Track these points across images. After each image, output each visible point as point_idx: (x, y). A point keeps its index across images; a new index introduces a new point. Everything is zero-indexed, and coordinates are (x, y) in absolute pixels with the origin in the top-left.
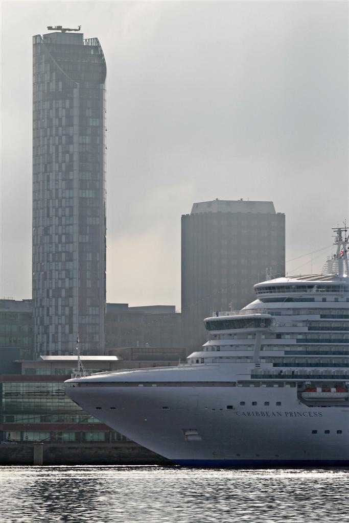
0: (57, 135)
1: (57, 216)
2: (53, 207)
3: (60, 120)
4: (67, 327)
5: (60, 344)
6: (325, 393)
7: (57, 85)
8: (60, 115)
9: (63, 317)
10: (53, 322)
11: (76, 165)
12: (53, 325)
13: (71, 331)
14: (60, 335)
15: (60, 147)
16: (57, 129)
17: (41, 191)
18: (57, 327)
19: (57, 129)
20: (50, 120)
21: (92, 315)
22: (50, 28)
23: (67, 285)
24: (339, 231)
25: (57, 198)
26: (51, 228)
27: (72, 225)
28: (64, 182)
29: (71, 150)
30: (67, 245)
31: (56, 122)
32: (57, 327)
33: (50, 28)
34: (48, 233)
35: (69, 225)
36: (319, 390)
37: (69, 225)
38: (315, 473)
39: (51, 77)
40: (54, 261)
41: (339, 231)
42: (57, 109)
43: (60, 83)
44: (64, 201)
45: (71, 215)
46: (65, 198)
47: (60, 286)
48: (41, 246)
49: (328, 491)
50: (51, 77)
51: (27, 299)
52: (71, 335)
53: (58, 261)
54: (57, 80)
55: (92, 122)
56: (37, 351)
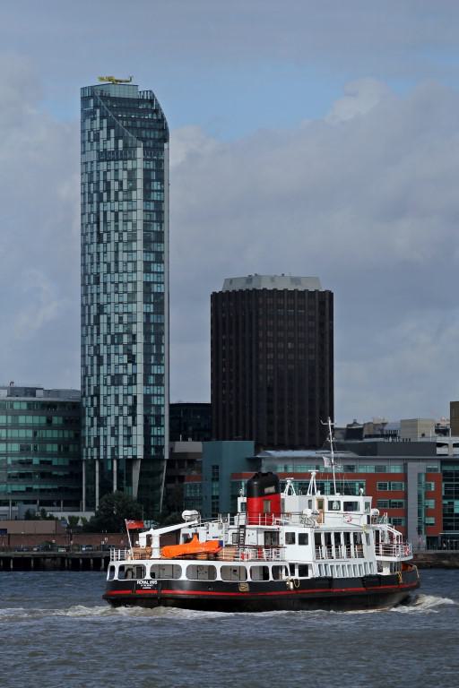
1: (116, 231)
3: (121, 184)
4: (130, 418)
7: (116, 143)
9: (125, 295)
10: (112, 239)
11: (140, 235)
12: (113, 243)
13: (134, 424)
16: (116, 193)
17: (95, 264)
19: (116, 193)
20: (108, 184)
21: (157, 273)
22: (102, 79)
23: (130, 371)
24: (355, 423)
26: (109, 418)
27: (136, 210)
29: (134, 218)
30: (130, 305)
31: (115, 186)
32: (117, 418)
33: (102, 79)
34: (105, 311)
38: (332, 421)
39: (109, 133)
40: (113, 384)
41: (355, 423)
42: (116, 171)
44: (121, 285)
45: (135, 271)
46: (122, 211)
47: (121, 372)
48: (95, 327)
50: (109, 133)
51: (80, 277)
52: (134, 428)
53: (118, 385)
55: (155, 370)
56: (89, 447)
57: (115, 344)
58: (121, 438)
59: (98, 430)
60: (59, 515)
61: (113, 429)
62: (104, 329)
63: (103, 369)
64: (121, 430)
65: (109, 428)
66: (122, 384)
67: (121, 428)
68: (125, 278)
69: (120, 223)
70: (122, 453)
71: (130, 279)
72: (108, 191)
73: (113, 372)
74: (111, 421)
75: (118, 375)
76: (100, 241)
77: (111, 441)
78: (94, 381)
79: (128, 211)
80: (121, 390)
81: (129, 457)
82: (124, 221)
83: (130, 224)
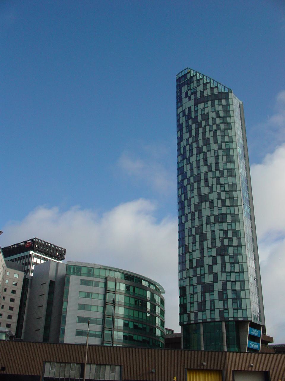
18: (224, 284)
46: (230, 281)
52: (243, 293)
57: (219, 223)
58: (230, 302)
59: (204, 296)
60: (165, 332)
61: (211, 268)
62: (206, 212)
63: (208, 244)
64: (230, 294)
65: (206, 267)
66: (226, 221)
67: (229, 292)
68: (233, 277)
69: (228, 266)
70: (230, 315)
71: (237, 278)
72: (207, 120)
73: (216, 212)
75: (222, 214)
76: (200, 150)
77: (219, 305)
78: (196, 255)
79: (235, 254)
80: (225, 226)
81: (240, 319)
82: (234, 309)
83: (236, 266)
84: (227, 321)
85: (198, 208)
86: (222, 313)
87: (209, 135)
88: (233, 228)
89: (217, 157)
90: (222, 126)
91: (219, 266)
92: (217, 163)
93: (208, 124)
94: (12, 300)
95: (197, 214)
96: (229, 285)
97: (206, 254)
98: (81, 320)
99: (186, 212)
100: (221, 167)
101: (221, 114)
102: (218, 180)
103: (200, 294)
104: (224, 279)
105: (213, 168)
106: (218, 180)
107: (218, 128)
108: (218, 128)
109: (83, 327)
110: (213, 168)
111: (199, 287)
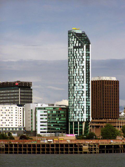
0: (70, 84)
2: (71, 44)
3: (80, 54)
4: (83, 112)
5: (80, 116)
6: (84, 67)
8: (80, 53)
14: (80, 114)
15: (80, 62)
18: (79, 112)
25: (79, 76)
28: (81, 71)
30: (82, 84)
32: (79, 112)
35: (83, 103)
36: (85, 148)
37: (83, 103)
43: (80, 44)
49: (84, 69)
54: (75, 38)
63: (75, 100)
67: (80, 114)
74: (77, 112)
84: (79, 122)
85: (73, 88)
86: (78, 119)
87: (77, 62)
88: (82, 85)
89: (79, 71)
90: (81, 60)
91: (78, 51)
92: (79, 74)
93: (77, 58)
94: (21, 116)
95: (73, 89)
96: (80, 112)
97: (75, 93)
98: (41, 122)
99: (70, 88)
100: (80, 75)
101: (81, 55)
102: (79, 79)
103: (73, 69)
104: (79, 110)
105: (78, 75)
106: (79, 79)
107: (80, 60)
108: (80, 60)
109: (42, 117)
110: (78, 75)
111: (73, 57)
